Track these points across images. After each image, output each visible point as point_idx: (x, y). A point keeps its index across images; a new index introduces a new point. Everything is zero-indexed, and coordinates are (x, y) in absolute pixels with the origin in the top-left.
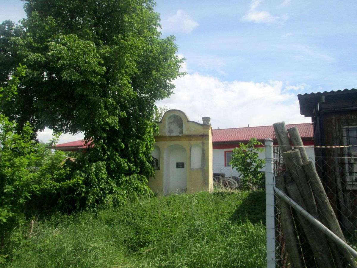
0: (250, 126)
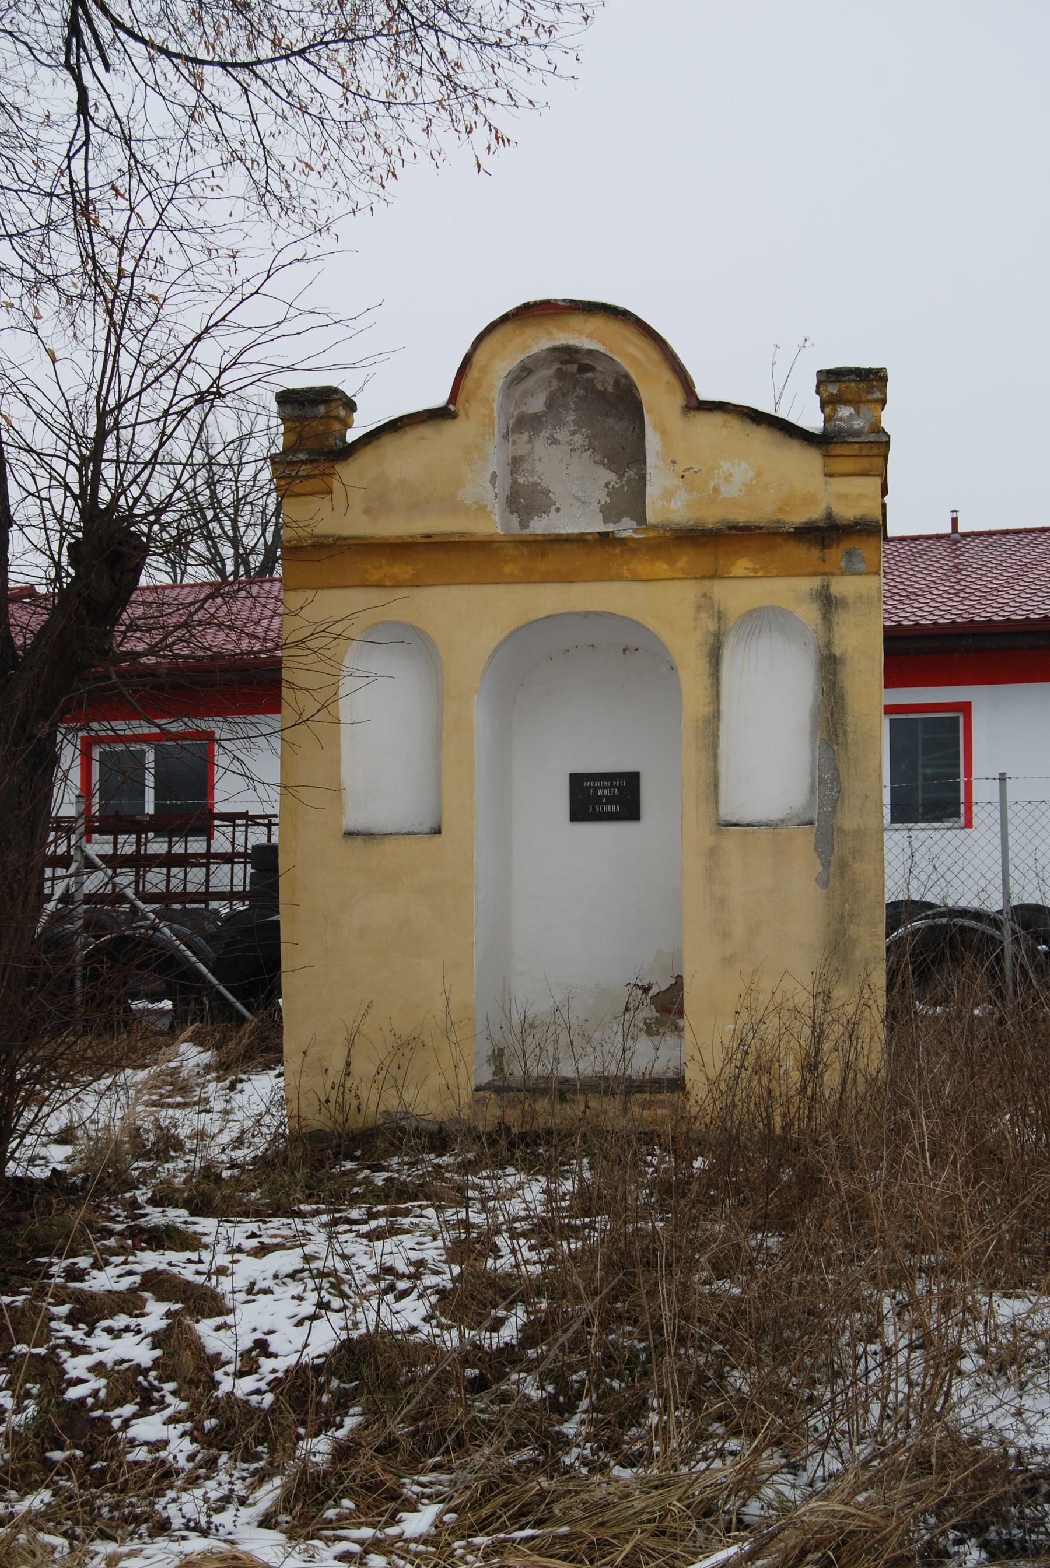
0: (962, 528)
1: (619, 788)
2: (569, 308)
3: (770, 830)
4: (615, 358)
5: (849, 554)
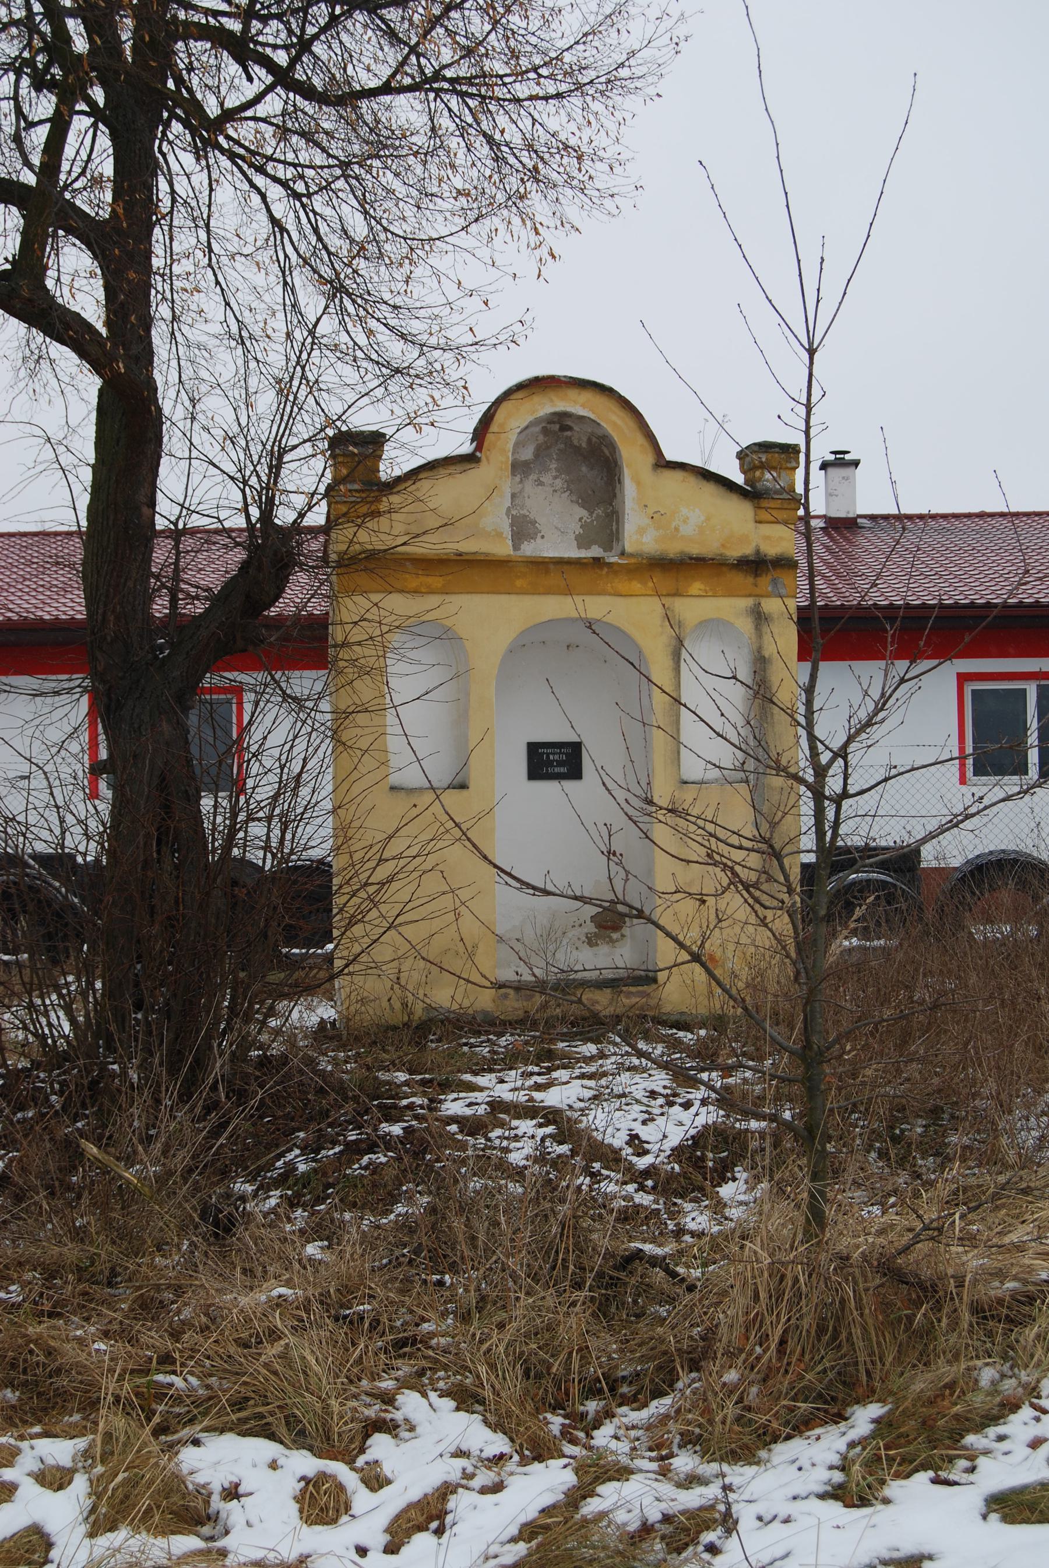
5: (774, 582)
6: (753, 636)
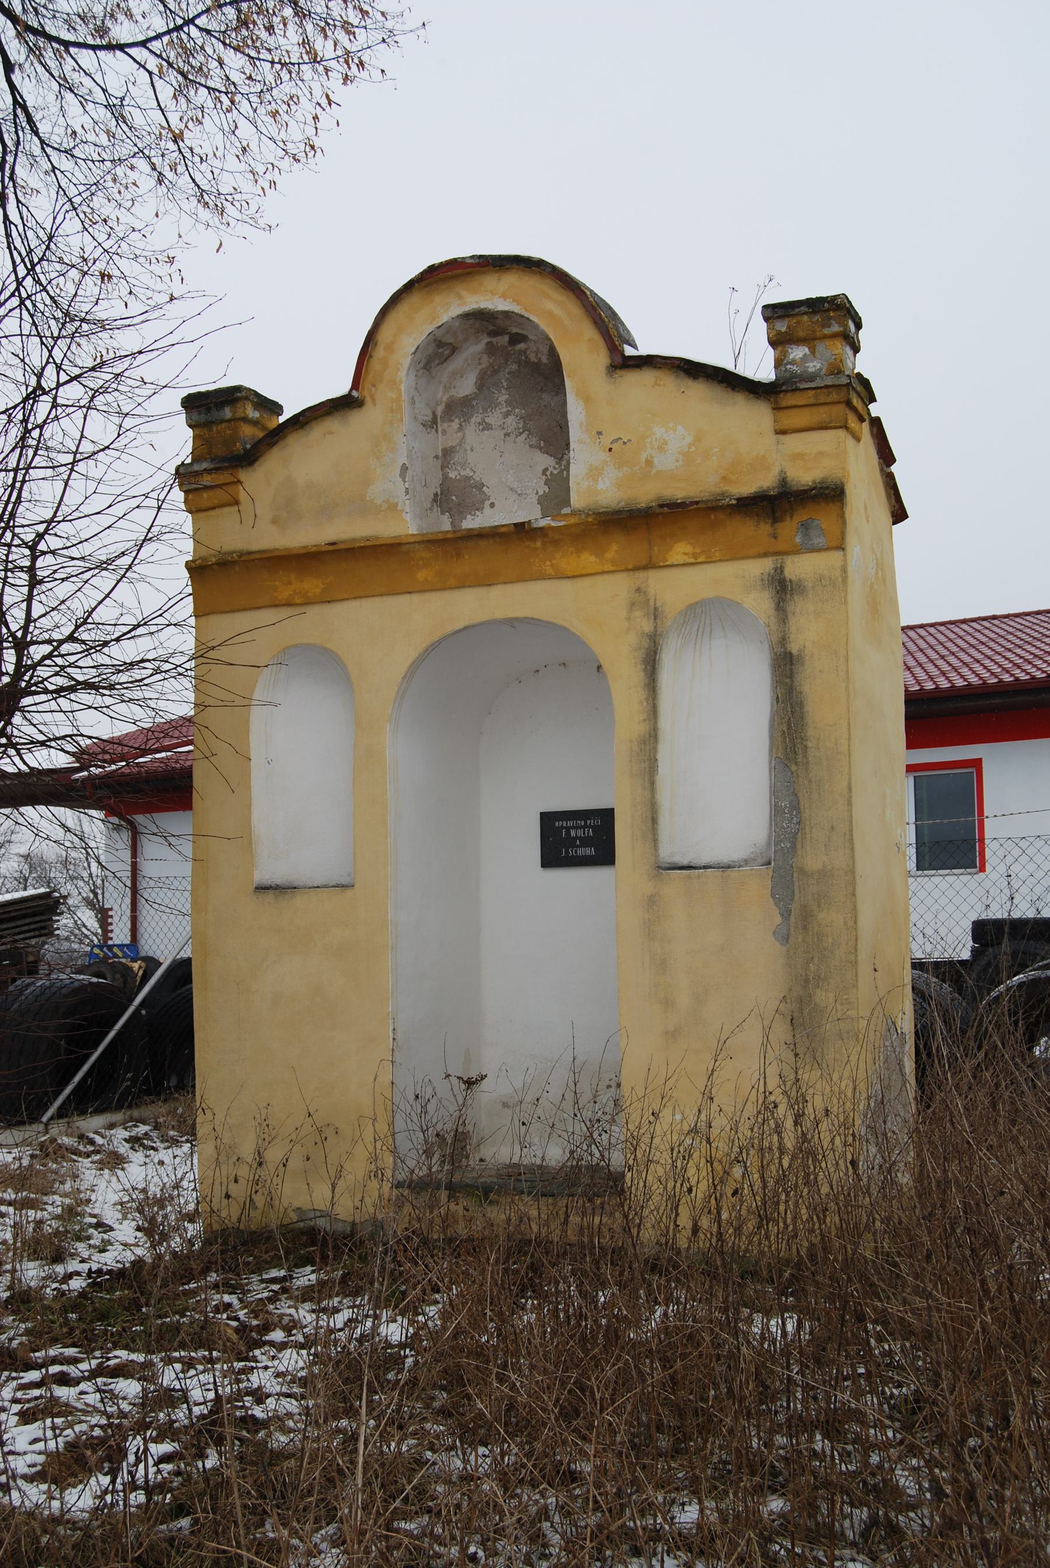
1: (594, 828)
2: (478, 265)
3: (718, 873)
4: (531, 318)
5: (805, 526)
6: (773, 621)
